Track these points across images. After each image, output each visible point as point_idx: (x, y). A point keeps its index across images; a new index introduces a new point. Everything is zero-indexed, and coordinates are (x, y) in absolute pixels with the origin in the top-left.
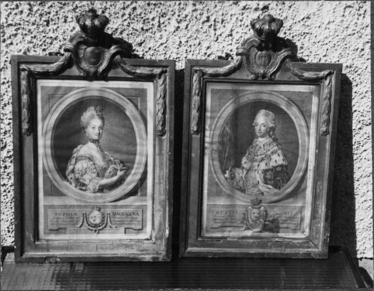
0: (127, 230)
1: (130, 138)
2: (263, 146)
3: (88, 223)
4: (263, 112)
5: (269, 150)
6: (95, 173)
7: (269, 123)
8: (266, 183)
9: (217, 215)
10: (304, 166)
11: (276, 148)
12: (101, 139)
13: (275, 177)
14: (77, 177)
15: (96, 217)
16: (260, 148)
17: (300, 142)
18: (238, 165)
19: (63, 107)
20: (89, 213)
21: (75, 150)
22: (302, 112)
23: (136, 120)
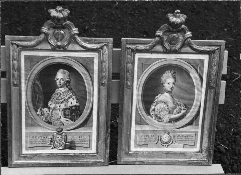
0: (185, 146)
1: (190, 91)
2: (62, 94)
3: (161, 141)
4: (61, 70)
5: (67, 96)
6: (167, 111)
7: (66, 78)
8: (65, 117)
9: (33, 139)
10: (91, 106)
11: (71, 94)
12: (173, 91)
13: (71, 114)
14: (156, 114)
15: (165, 138)
16: (61, 94)
17: (87, 90)
18: (46, 105)
19: (151, 70)
20: (162, 135)
21: (156, 97)
22: (87, 70)
23: (195, 78)
